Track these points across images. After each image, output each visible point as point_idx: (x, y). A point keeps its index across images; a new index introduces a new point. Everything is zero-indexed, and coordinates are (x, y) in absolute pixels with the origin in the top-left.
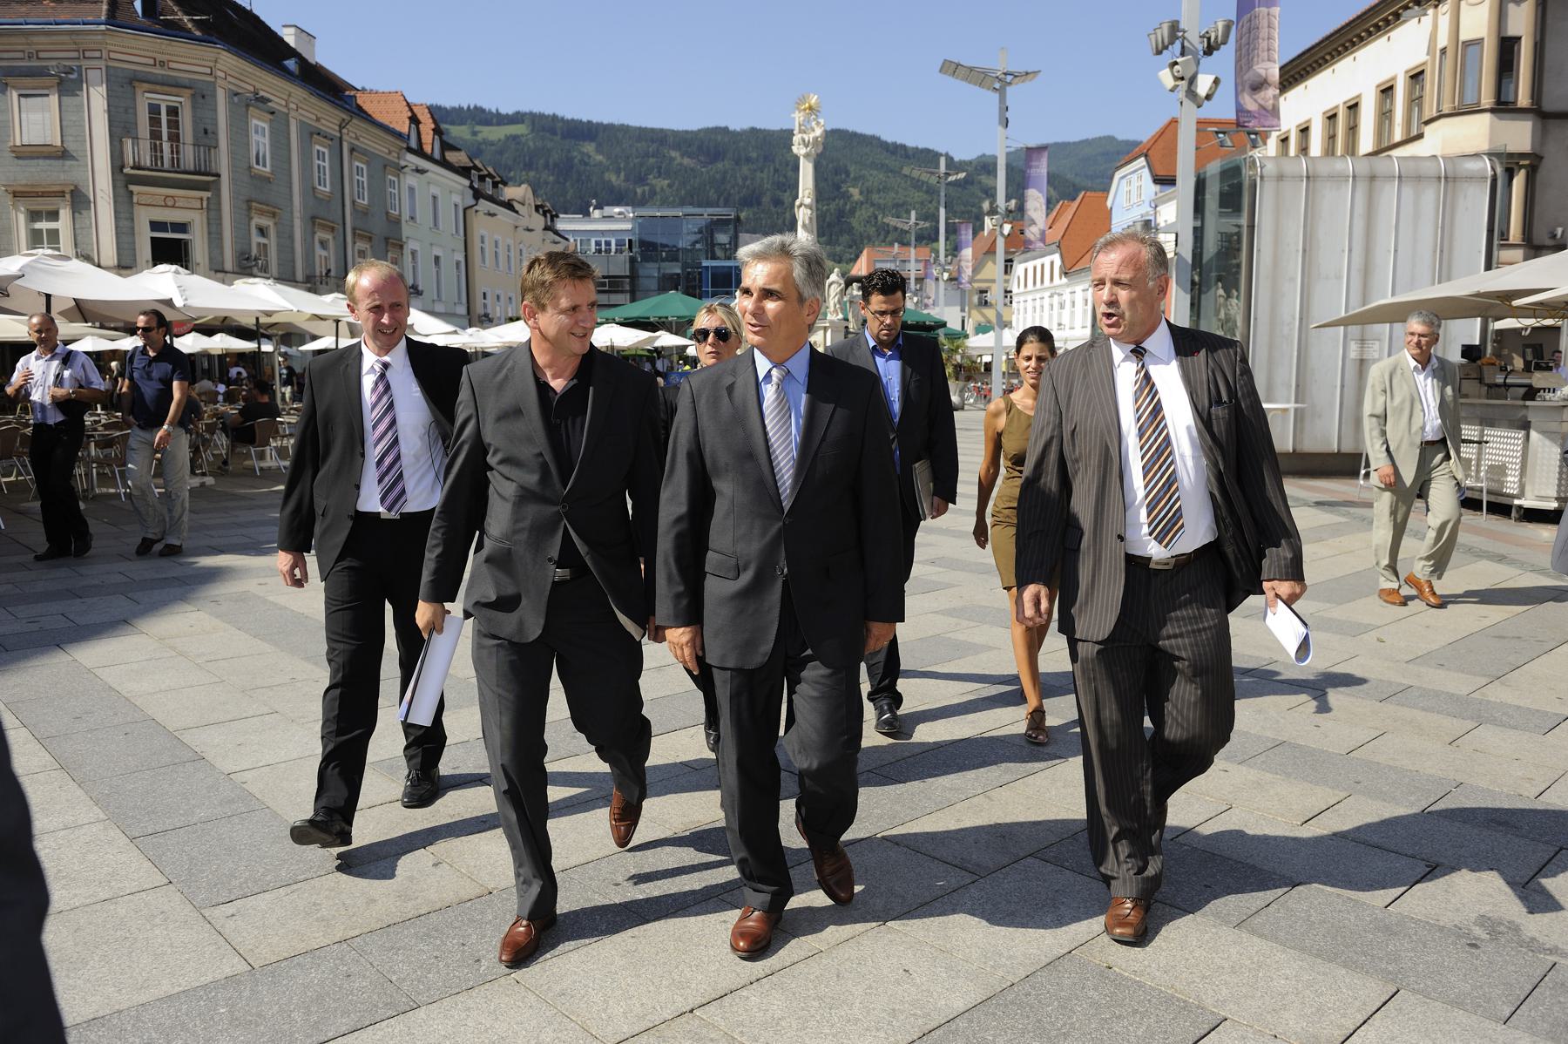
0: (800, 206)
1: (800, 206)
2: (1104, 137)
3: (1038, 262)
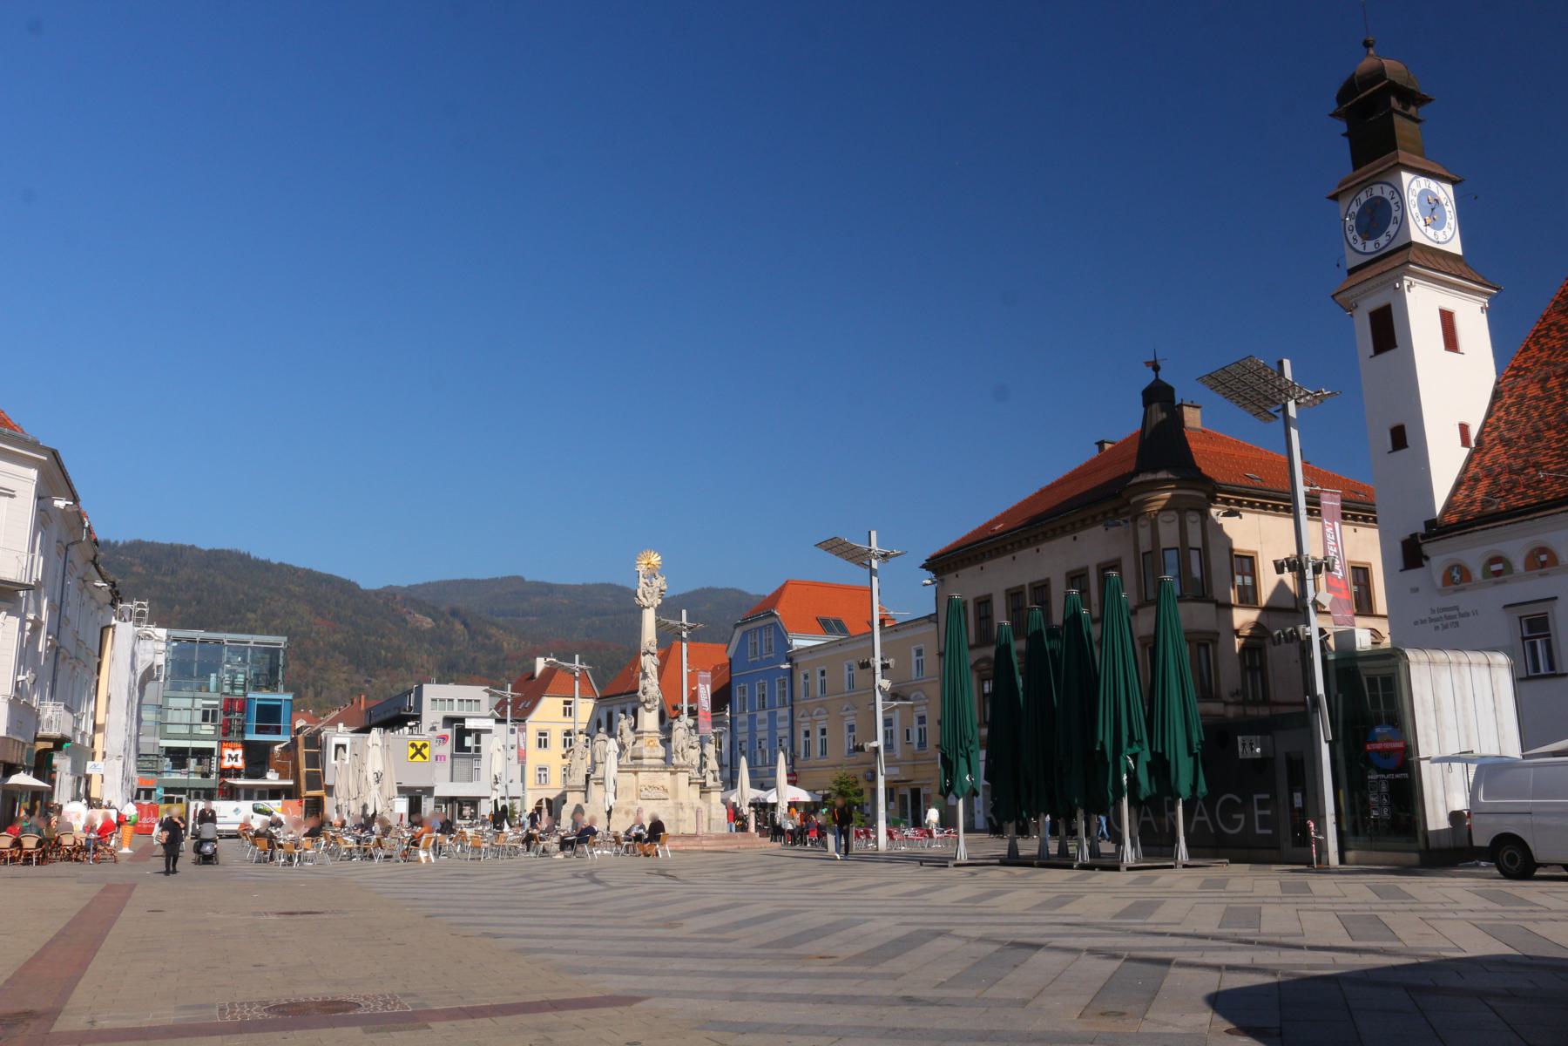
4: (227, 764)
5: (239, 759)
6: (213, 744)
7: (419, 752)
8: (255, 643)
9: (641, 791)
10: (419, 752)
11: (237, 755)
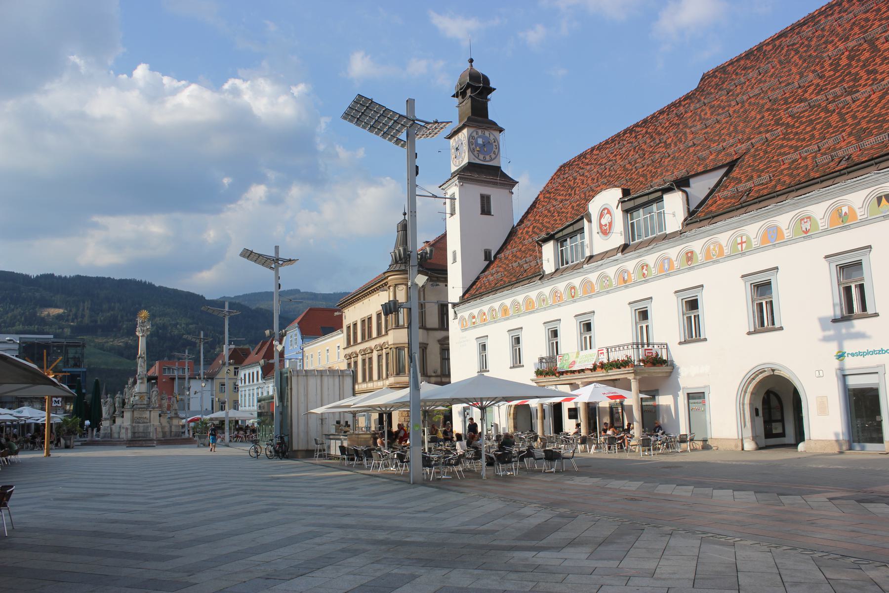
0: (139, 358)
1: (139, 358)
2: (294, 290)
3: (251, 371)
8: (67, 343)
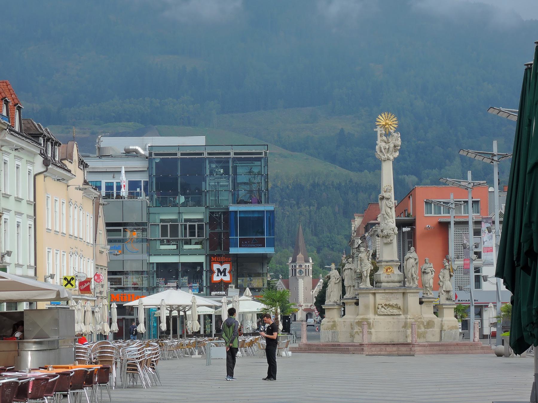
4: (216, 278)
5: (227, 274)
6: (201, 259)
7: (69, 282)
9: (378, 308)
10: (69, 282)
11: (225, 269)
